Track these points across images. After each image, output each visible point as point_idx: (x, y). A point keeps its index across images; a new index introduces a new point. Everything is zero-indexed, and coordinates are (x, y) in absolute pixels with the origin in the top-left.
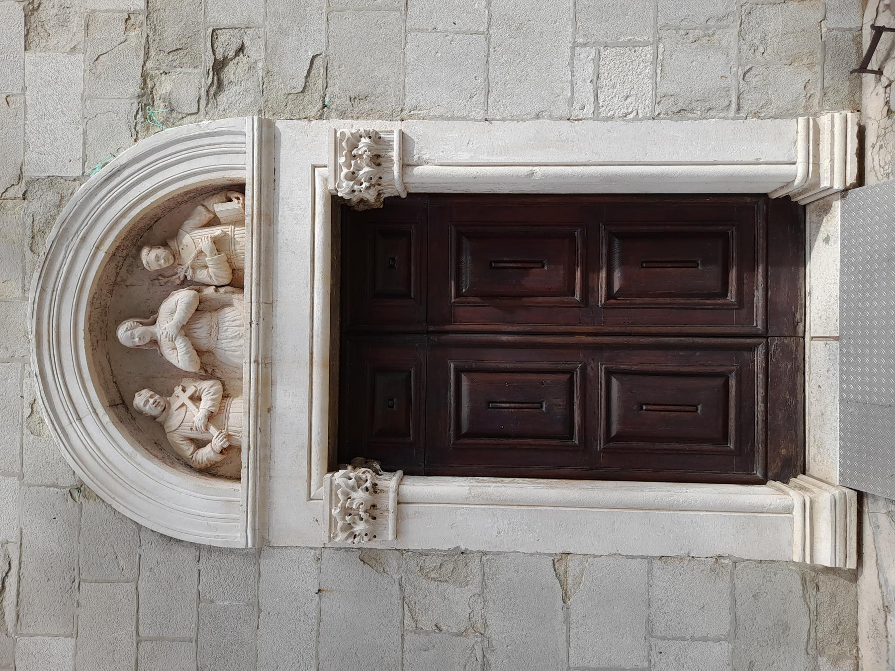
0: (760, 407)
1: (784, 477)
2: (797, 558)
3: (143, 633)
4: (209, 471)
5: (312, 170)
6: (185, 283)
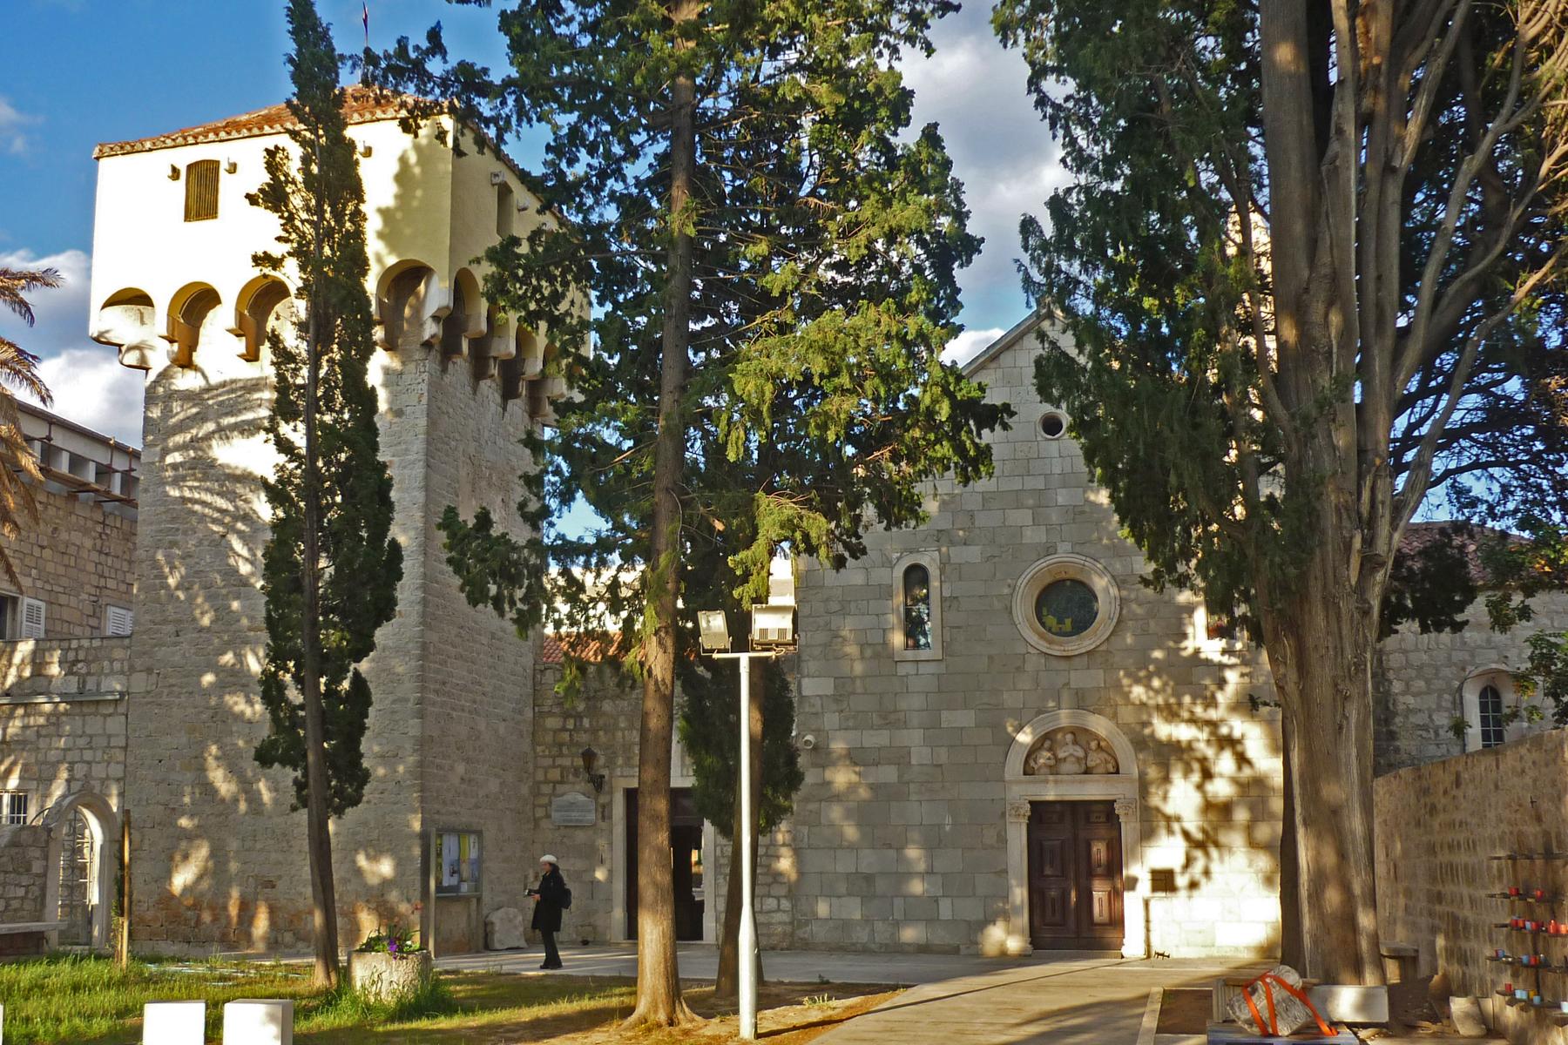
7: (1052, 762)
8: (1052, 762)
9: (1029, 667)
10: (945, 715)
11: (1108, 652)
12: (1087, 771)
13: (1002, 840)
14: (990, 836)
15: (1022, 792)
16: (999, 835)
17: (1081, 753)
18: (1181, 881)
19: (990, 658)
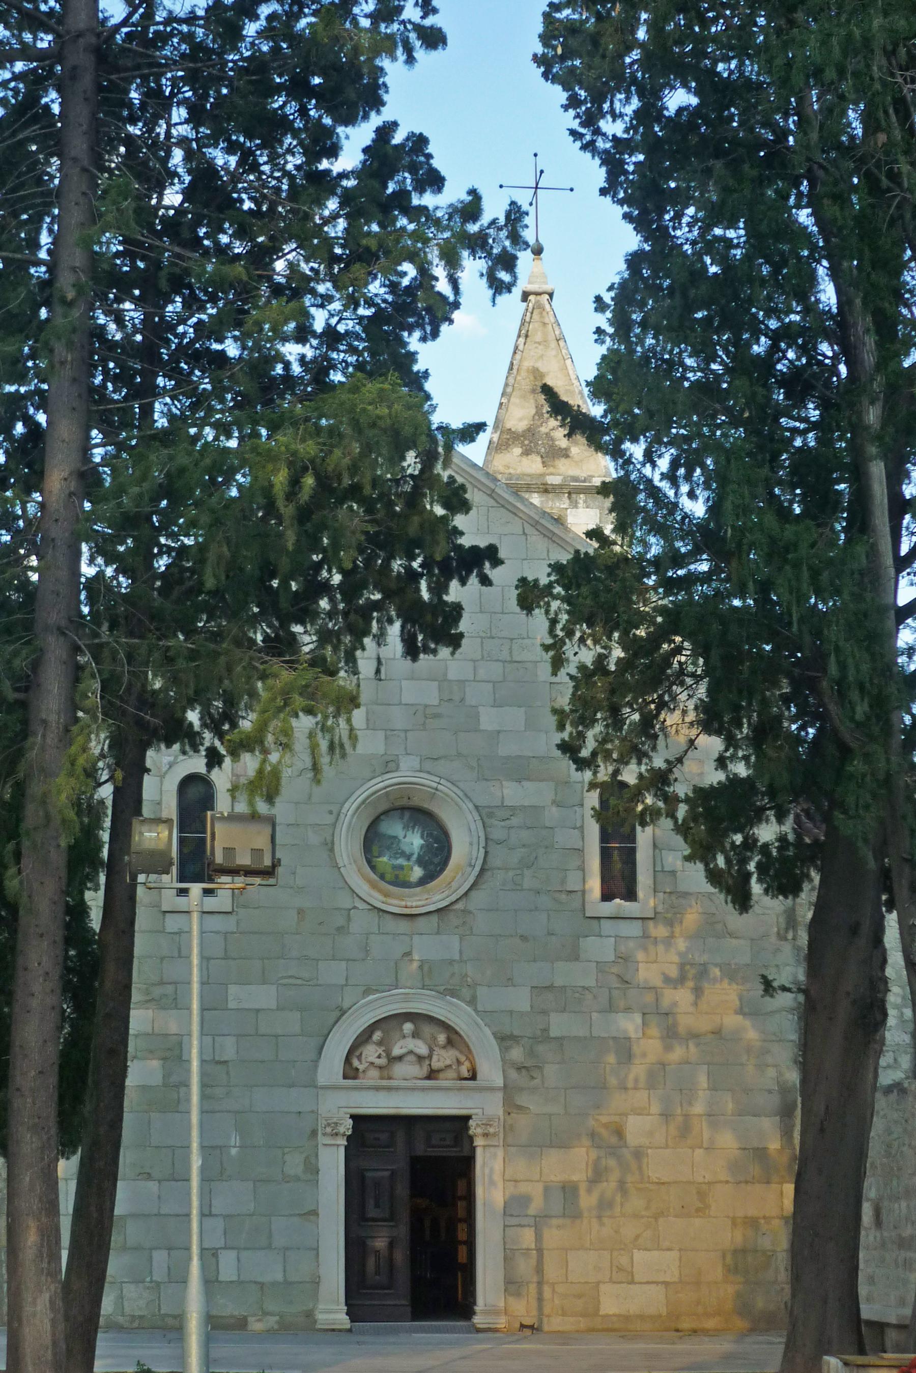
0: (368, 1303)
1: (464, 1166)
2: (321, 1306)
3: (212, 961)
4: (348, 1061)
5: (481, 1107)
6: (431, 1050)
7: (383, 1061)
8: (383, 1061)
9: (354, 927)
10: (233, 989)
11: (465, 912)
12: (432, 1075)
13: (312, 1169)
14: (294, 1164)
15: (342, 1105)
16: (307, 1161)
17: (423, 1050)
18: (587, 1201)
19: (300, 912)
